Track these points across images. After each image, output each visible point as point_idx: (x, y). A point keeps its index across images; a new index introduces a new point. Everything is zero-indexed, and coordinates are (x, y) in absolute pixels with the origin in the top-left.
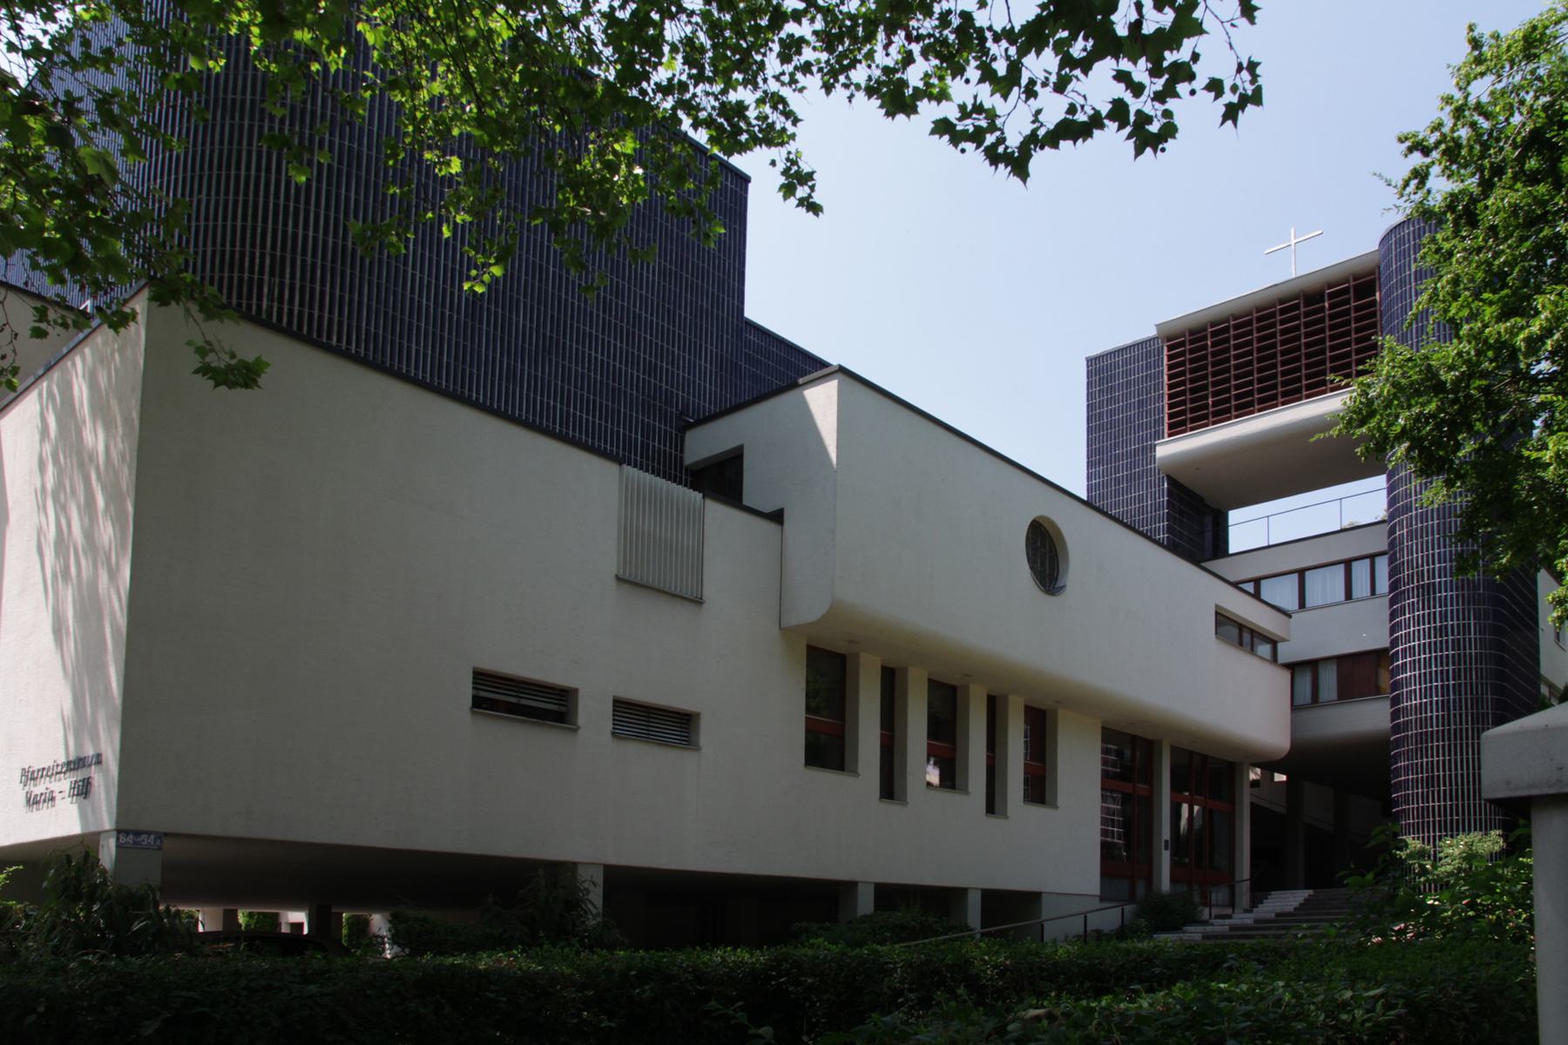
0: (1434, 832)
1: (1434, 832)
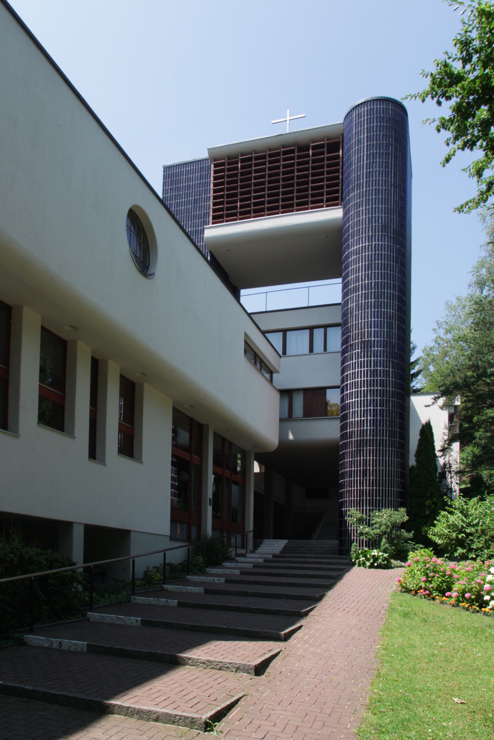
0: (366, 506)
1: (366, 506)
